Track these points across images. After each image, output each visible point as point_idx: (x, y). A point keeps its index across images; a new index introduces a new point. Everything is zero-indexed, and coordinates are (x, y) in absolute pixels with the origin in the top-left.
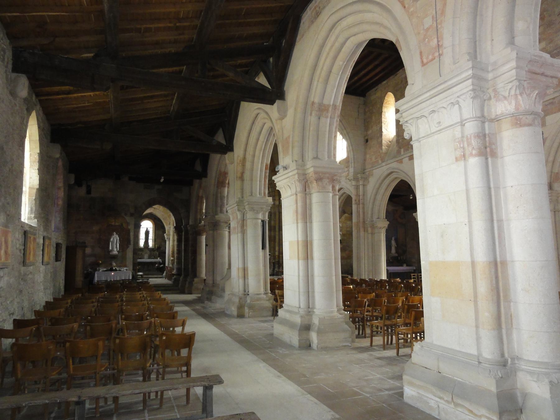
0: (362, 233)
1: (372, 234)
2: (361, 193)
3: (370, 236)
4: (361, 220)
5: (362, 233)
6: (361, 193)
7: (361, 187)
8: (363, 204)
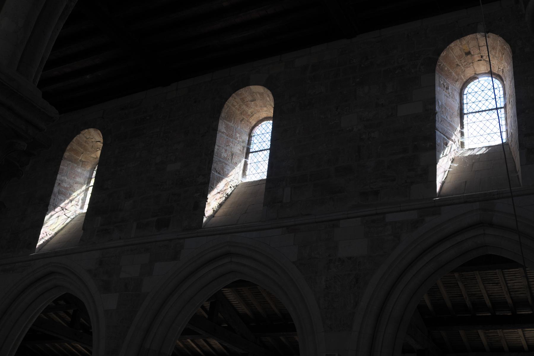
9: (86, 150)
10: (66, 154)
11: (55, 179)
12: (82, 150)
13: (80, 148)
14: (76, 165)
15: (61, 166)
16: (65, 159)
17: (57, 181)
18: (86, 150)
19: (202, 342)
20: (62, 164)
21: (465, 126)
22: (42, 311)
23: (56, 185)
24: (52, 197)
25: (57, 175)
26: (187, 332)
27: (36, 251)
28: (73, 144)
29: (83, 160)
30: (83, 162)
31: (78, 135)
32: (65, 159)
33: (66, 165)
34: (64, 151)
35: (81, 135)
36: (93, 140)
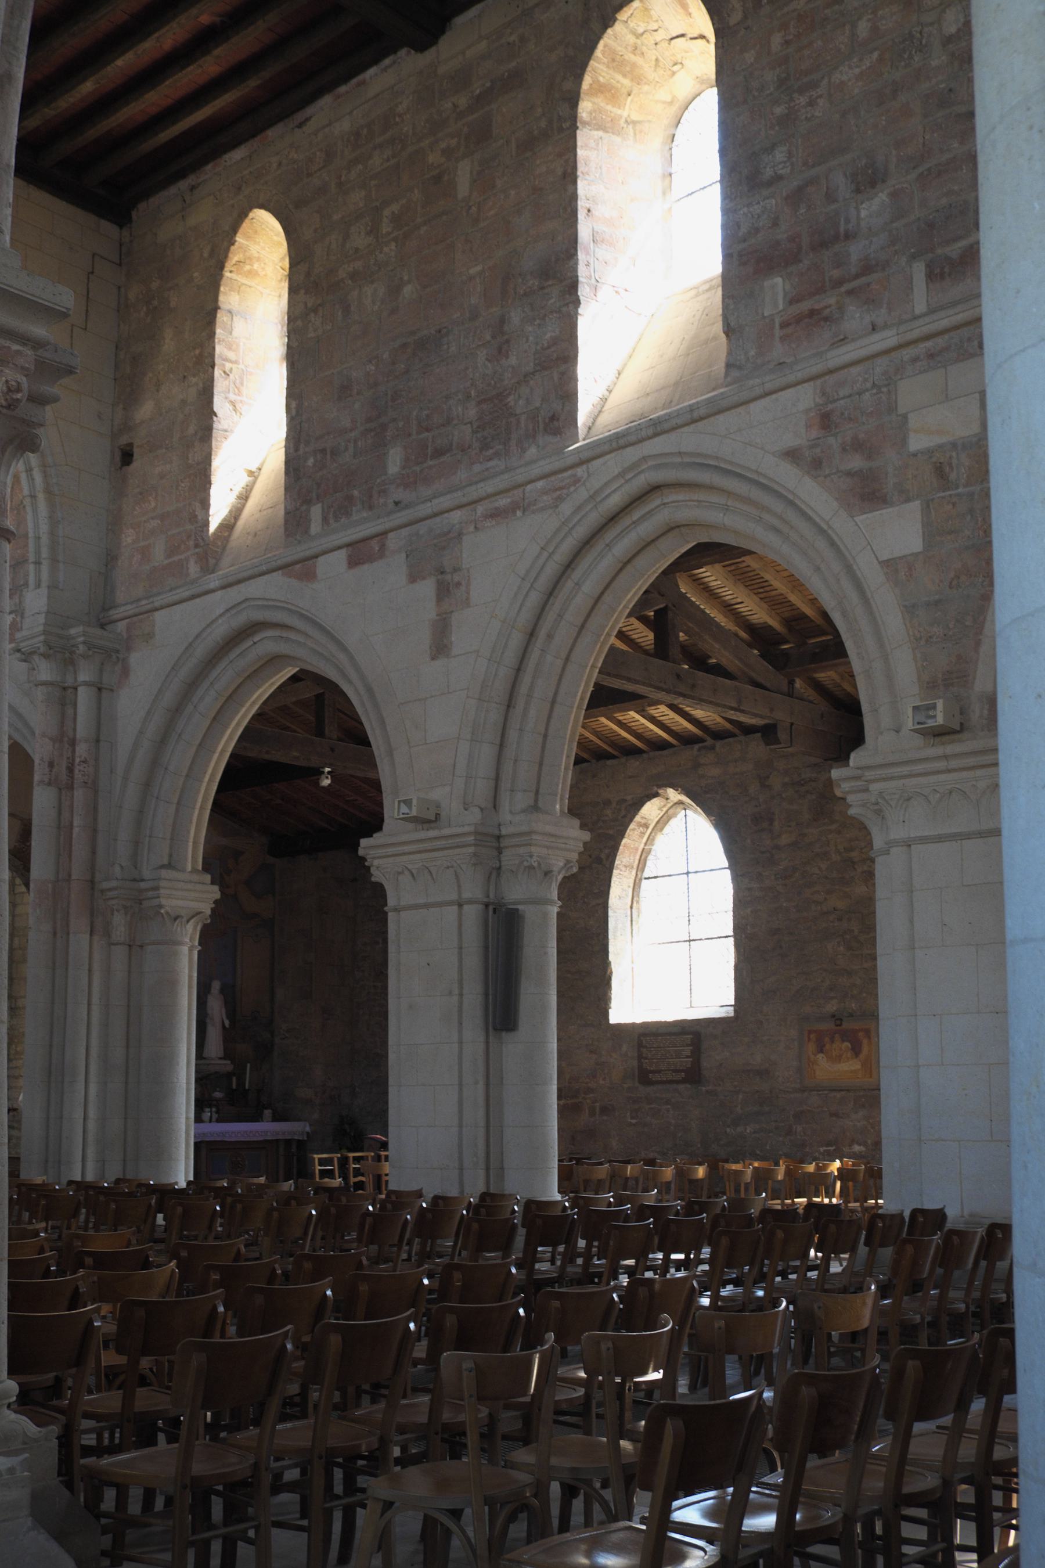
0: (80, 941)
1: (135, 946)
2: (83, 727)
3: (120, 953)
4: (78, 872)
5: (80, 941)
6: (83, 727)
7: (84, 697)
8: (93, 786)
9: (638, 79)
10: (585, 108)
11: (574, 197)
12: (626, 82)
13: (619, 77)
14: (617, 139)
15: (580, 152)
16: (586, 124)
17: (582, 204)
18: (638, 79)
19: (662, 711)
20: (579, 143)
21: (238, 489)
22: (628, 611)
23: (581, 215)
24: (581, 256)
25: (575, 183)
26: (604, 698)
27: (582, 430)
28: (599, 69)
29: (635, 117)
30: (634, 123)
31: (609, 31)
32: (586, 124)
33: (592, 144)
34: (573, 100)
35: (618, 27)
36: (660, 36)
